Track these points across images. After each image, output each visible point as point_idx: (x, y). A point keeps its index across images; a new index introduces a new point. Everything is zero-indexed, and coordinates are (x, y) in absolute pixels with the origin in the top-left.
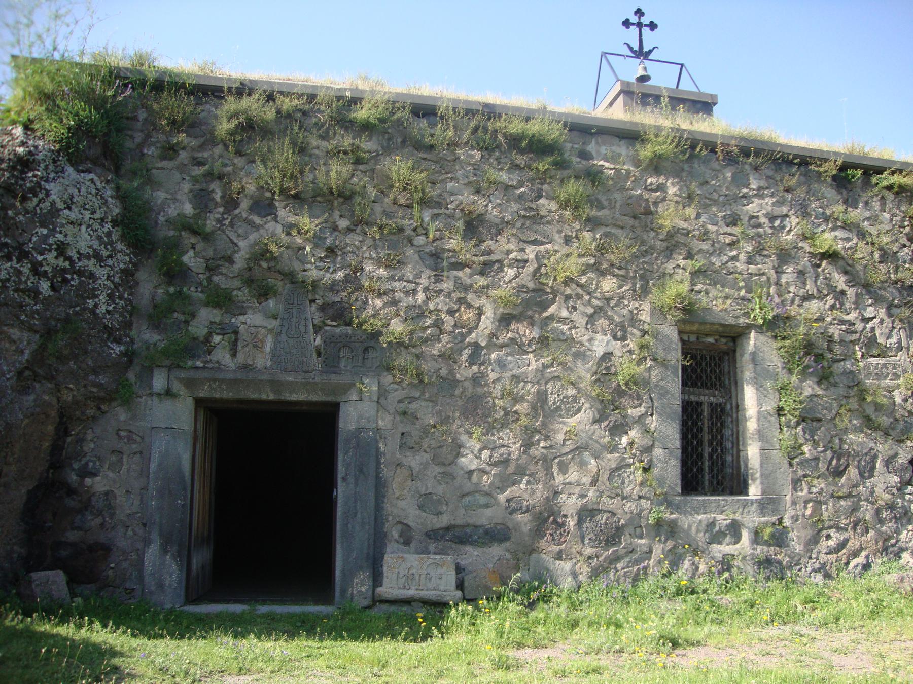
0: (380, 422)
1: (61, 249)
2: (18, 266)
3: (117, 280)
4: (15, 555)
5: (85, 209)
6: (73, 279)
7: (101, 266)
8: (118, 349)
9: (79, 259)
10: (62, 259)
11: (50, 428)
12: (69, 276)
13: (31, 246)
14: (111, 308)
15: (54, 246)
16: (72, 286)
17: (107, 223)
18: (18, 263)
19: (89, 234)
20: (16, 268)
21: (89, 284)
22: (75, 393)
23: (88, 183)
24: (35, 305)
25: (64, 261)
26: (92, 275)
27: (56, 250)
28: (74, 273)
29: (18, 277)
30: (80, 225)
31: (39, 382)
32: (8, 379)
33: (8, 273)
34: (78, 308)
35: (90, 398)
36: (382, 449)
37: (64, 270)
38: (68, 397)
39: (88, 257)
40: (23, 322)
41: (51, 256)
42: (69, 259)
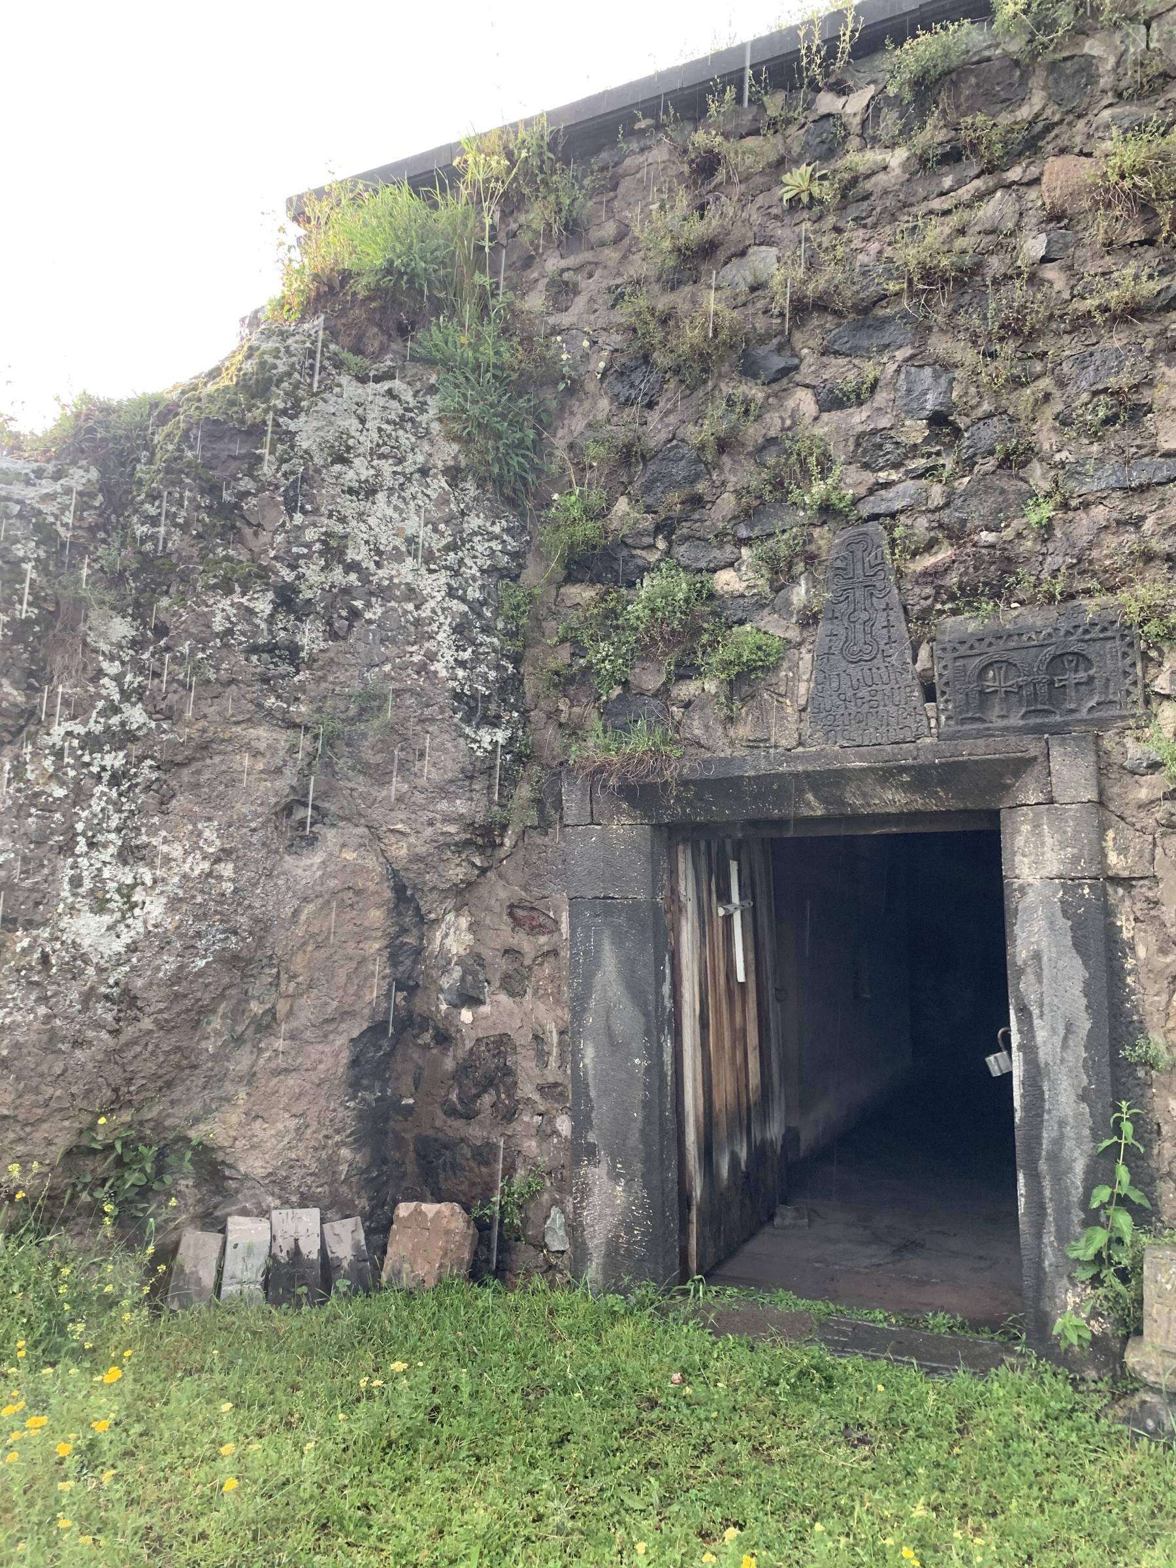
0: (1112, 858)
1: (333, 551)
2: (243, 600)
3: (474, 593)
4: (344, 1168)
5: (382, 456)
6: (368, 605)
7: (431, 571)
8: (487, 739)
9: (378, 565)
10: (339, 570)
11: (376, 916)
12: (359, 604)
13: (272, 554)
14: (466, 655)
15: (317, 546)
16: (370, 622)
17: (435, 476)
18: (244, 594)
19: (396, 508)
20: (239, 606)
21: (406, 612)
22: (412, 840)
23: (381, 401)
24: (297, 673)
25: (347, 573)
26: (411, 593)
27: (321, 553)
28: (372, 594)
29: (249, 622)
30: (374, 492)
31: (333, 825)
32: (254, 830)
33: (228, 618)
34: (387, 668)
35: (448, 845)
36: (1126, 935)
37: (347, 591)
38: (400, 851)
39: (398, 557)
40: (270, 713)
41: (313, 572)
42: (352, 567)
